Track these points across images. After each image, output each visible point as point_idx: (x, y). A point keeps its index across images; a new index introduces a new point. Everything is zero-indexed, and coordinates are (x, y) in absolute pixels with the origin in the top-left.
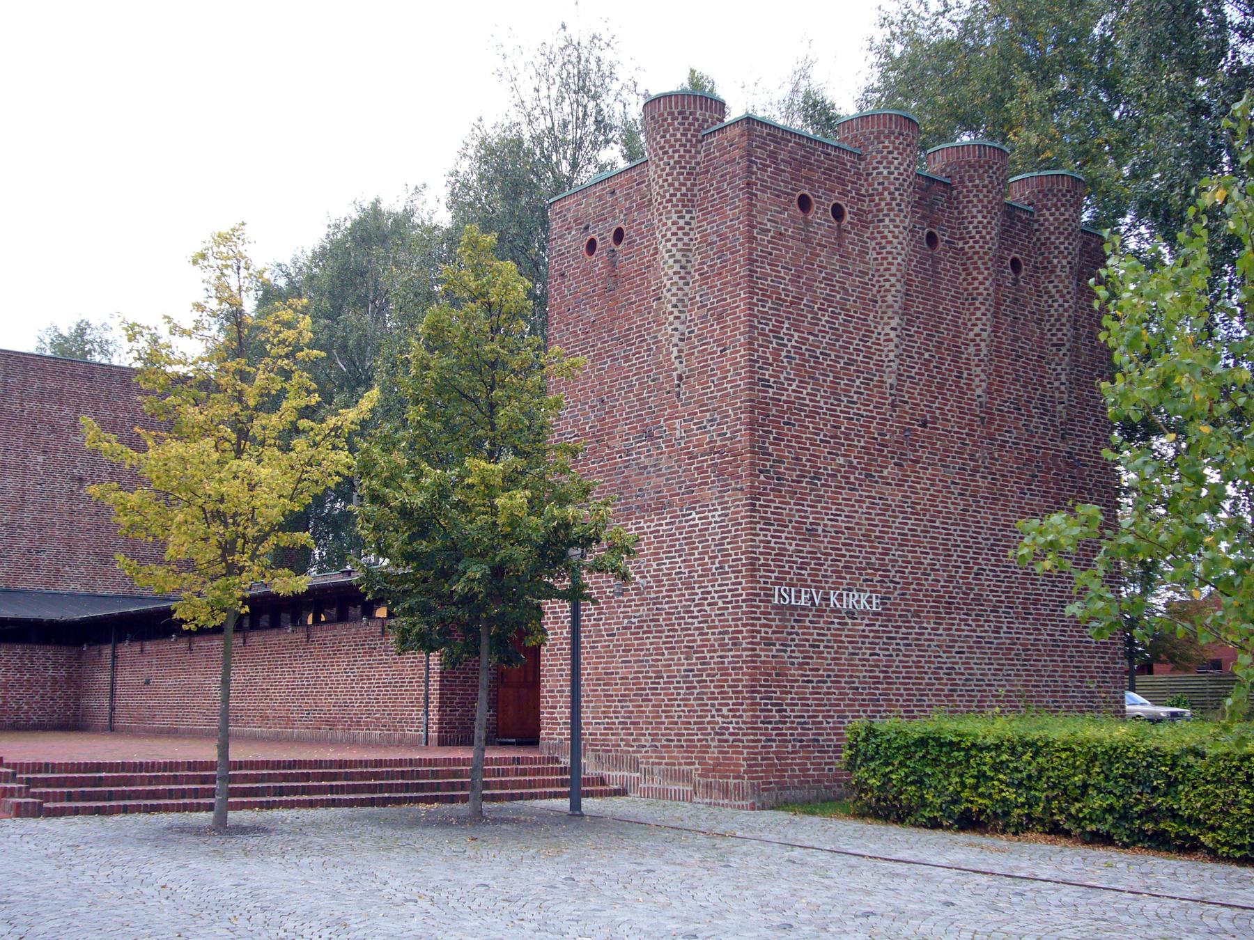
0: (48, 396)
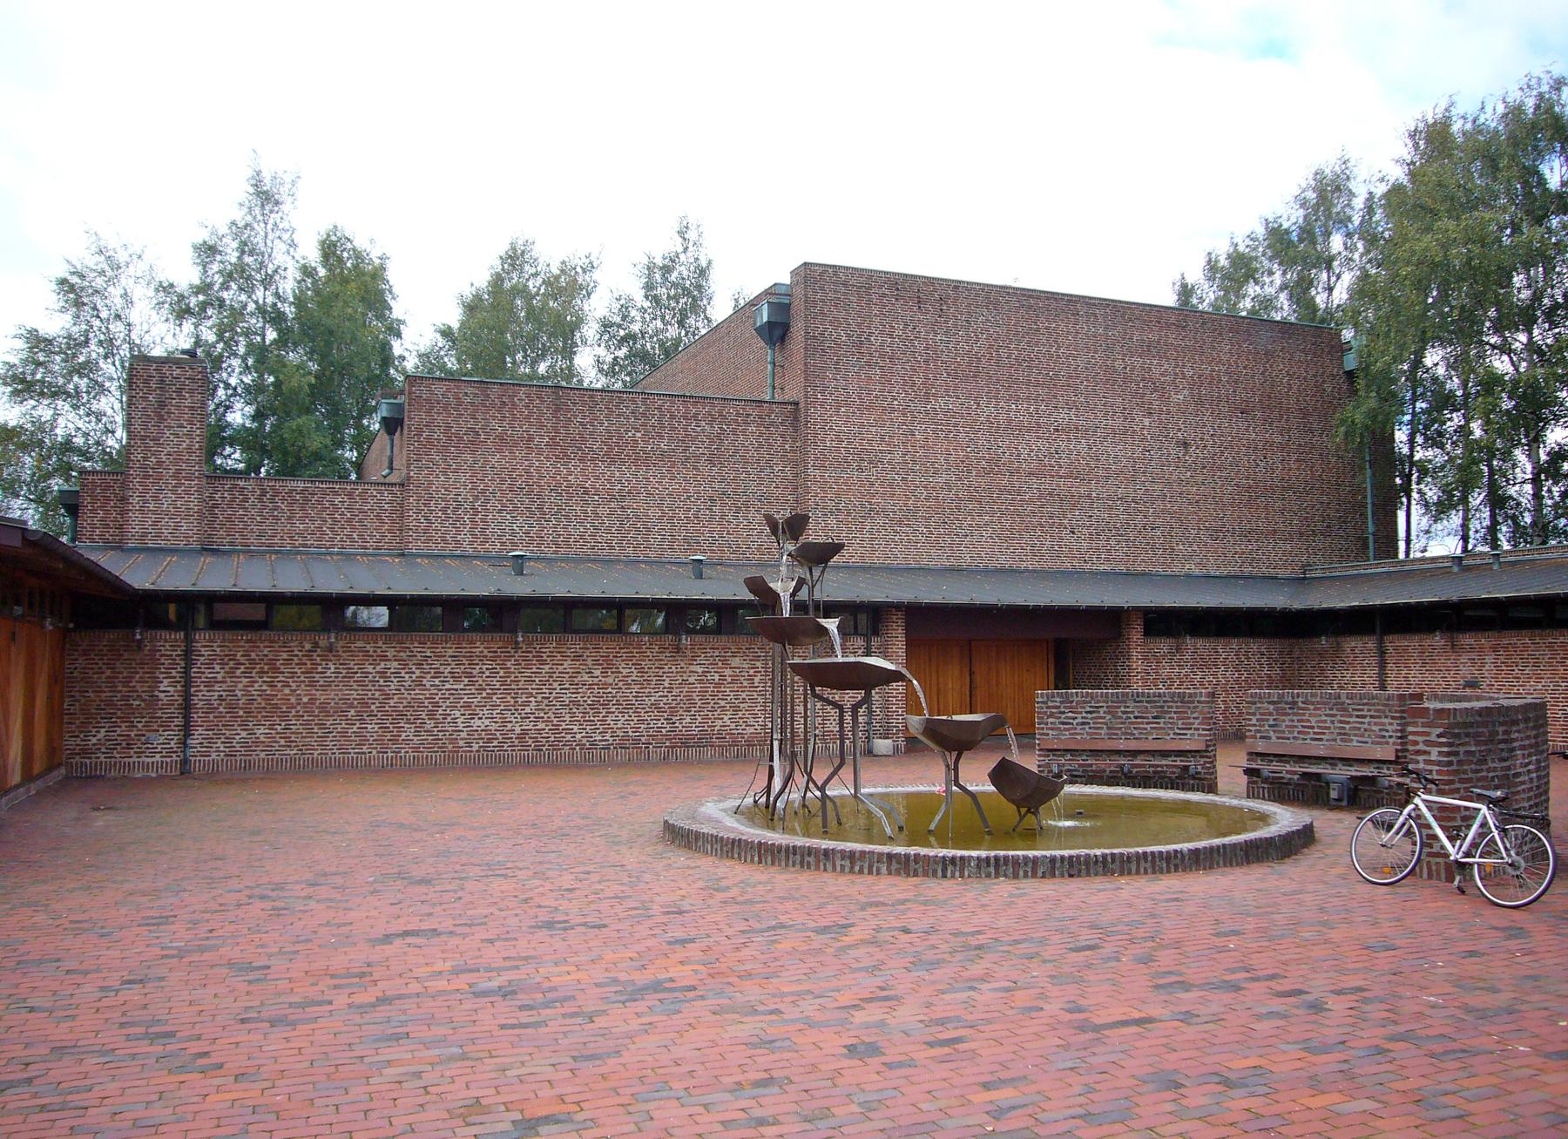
0: (1147, 349)
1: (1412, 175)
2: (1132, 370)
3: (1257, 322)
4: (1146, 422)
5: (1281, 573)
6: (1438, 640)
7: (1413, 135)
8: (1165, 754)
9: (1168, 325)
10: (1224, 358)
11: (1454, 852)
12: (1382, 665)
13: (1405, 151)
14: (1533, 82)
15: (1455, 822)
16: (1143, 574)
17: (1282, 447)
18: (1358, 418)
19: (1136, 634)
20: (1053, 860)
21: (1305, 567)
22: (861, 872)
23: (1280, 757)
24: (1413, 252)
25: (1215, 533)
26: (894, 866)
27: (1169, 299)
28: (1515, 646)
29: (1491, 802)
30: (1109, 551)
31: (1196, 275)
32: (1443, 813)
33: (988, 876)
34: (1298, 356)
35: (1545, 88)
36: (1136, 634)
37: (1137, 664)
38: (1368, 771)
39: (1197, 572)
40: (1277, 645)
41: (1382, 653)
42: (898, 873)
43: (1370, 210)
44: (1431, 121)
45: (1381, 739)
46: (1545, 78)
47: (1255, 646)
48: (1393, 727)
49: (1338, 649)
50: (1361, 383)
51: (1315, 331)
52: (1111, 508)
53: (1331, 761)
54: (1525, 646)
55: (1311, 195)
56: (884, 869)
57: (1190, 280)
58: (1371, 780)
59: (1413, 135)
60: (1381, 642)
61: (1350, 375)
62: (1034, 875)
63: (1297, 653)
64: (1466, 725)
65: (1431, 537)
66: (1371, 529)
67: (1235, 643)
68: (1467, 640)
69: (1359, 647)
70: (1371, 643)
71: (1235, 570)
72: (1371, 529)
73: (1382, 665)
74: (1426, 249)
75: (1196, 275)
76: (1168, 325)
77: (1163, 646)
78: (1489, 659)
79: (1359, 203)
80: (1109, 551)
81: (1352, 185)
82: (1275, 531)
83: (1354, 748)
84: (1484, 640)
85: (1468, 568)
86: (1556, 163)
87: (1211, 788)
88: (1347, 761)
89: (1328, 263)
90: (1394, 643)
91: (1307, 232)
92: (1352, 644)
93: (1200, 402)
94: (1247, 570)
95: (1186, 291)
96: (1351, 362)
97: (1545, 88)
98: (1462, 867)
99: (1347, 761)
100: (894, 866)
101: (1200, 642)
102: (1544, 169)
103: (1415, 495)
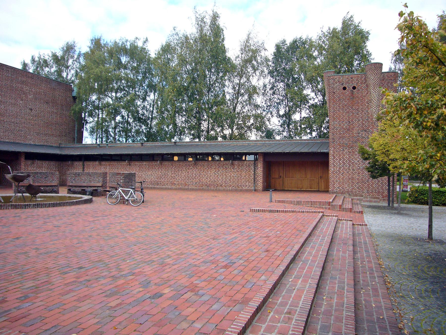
0: (22, 83)
1: (91, 50)
2: (18, 87)
3: (47, 80)
4: (21, 102)
5: (54, 145)
6: (97, 163)
7: (92, 40)
8: (47, 186)
9: (29, 77)
10: (43, 88)
11: (126, 198)
12: (84, 168)
13: (89, 44)
14: (122, 39)
15: (126, 193)
16: (18, 143)
17: (56, 113)
18: (77, 109)
19: (23, 159)
20: (49, 204)
21: (60, 144)
22: (4, 209)
23: (75, 186)
24: (94, 72)
25: (38, 134)
26: (13, 207)
27: (20, 67)
28: (113, 165)
29: (132, 188)
30: (8, 136)
31: (28, 61)
32: (123, 191)
33: (35, 208)
34: (61, 90)
35: (124, 41)
36: (23, 159)
37: (23, 167)
38: (95, 188)
39: (32, 143)
40: (57, 163)
41: (84, 165)
42: (14, 208)
43: (79, 55)
44: (96, 38)
45: (99, 182)
46: (124, 39)
47: (52, 163)
48: (101, 179)
49: (73, 164)
50: (77, 100)
51: (66, 86)
52: (10, 124)
53: (87, 187)
54: (116, 165)
55: (65, 49)
56: (10, 208)
57: (26, 62)
58: (96, 190)
59: (92, 40)
60: (84, 163)
61: (74, 98)
62: (46, 207)
63: (62, 165)
64: (127, 176)
65: (88, 139)
66: (76, 136)
67: (47, 162)
68: (103, 163)
69: (78, 164)
70: (81, 163)
71: (42, 143)
72: (76, 136)
73: (84, 168)
74: (97, 72)
75: (28, 61)
76: (29, 77)
77: (29, 162)
78: (108, 167)
79: (77, 53)
80: (8, 136)
81: (76, 48)
82: (53, 134)
83: (92, 184)
84: (107, 163)
85: (101, 147)
86: (125, 58)
87: (58, 193)
88: (91, 187)
89: (67, 67)
90: (87, 163)
91: (63, 58)
92: (77, 163)
93: (36, 99)
94: (46, 144)
95: (25, 65)
96: (74, 94)
97: (124, 41)
98: (127, 200)
99: (91, 187)
100: (13, 207)
101: (39, 162)
102: (122, 58)
103: (85, 128)
